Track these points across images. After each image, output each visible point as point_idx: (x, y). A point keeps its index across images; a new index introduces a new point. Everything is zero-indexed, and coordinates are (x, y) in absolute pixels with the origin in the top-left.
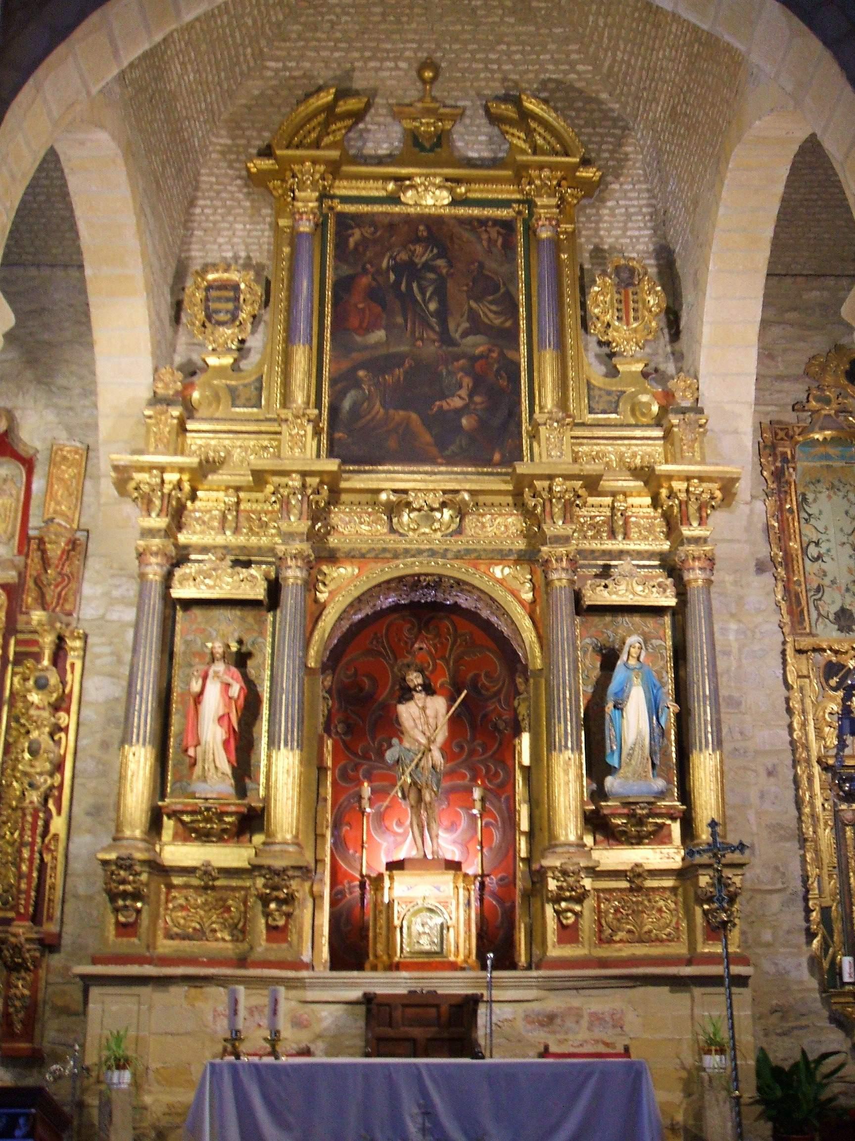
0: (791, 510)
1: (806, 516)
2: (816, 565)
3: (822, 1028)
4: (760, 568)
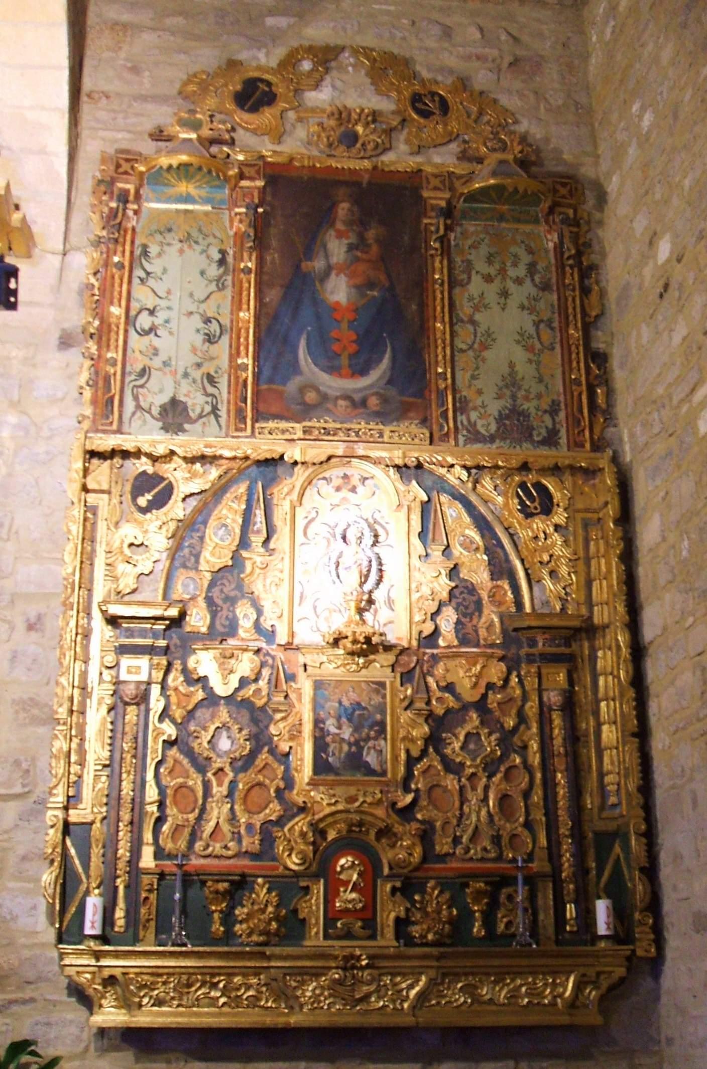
0: (120, 266)
1: (143, 275)
2: (146, 340)
3: (55, 1003)
4: (66, 342)
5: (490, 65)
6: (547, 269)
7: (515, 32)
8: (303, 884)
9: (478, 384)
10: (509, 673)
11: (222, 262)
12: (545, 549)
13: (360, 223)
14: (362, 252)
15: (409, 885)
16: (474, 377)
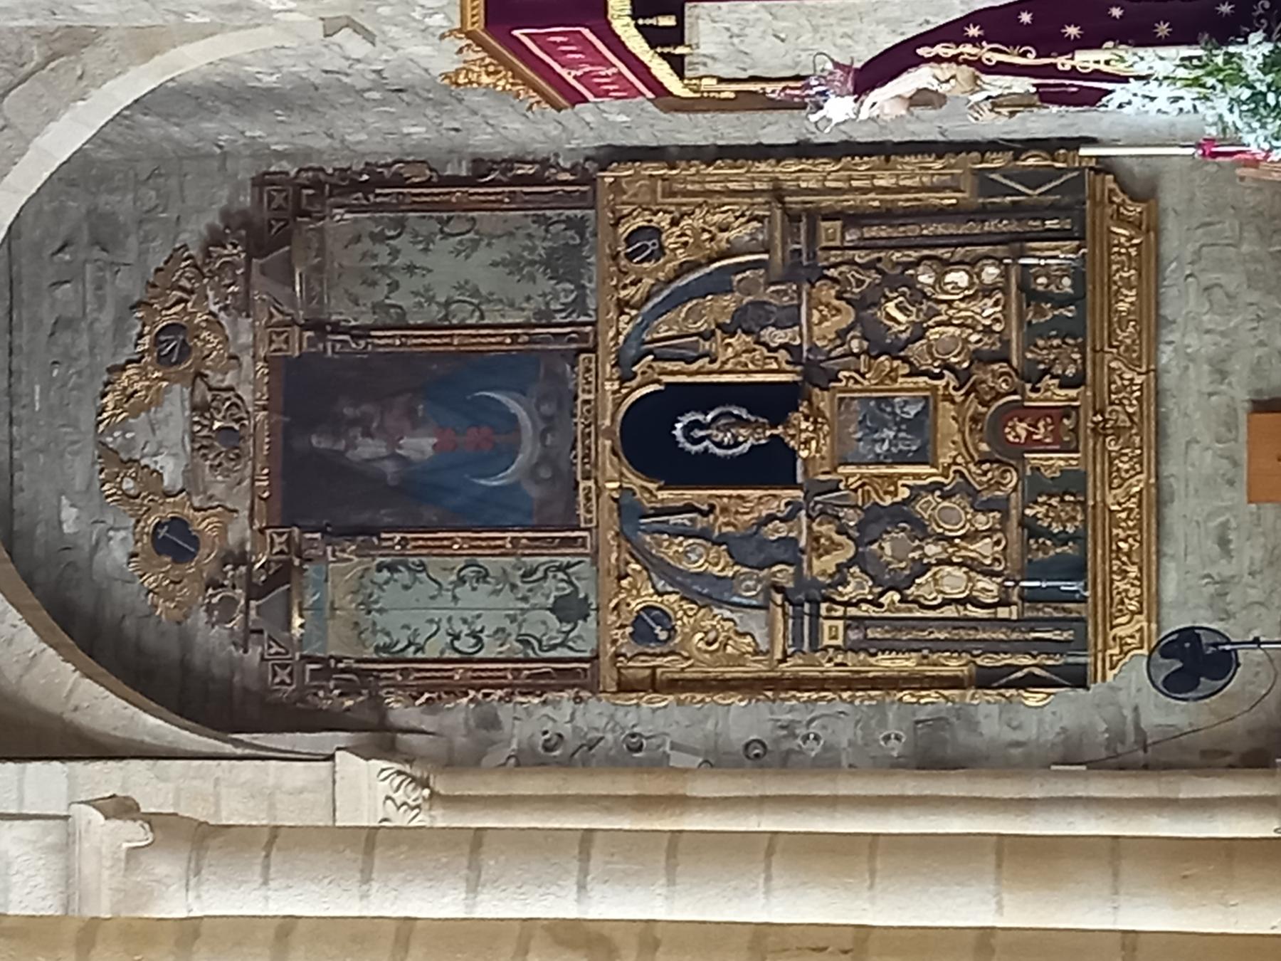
5: (108, 275)
6: (377, 222)
7: (58, 245)
8: (1029, 472)
9: (519, 301)
10: (826, 277)
11: (392, 568)
12: (696, 235)
13: (338, 427)
14: (372, 422)
15: (1032, 375)
16: (512, 305)
